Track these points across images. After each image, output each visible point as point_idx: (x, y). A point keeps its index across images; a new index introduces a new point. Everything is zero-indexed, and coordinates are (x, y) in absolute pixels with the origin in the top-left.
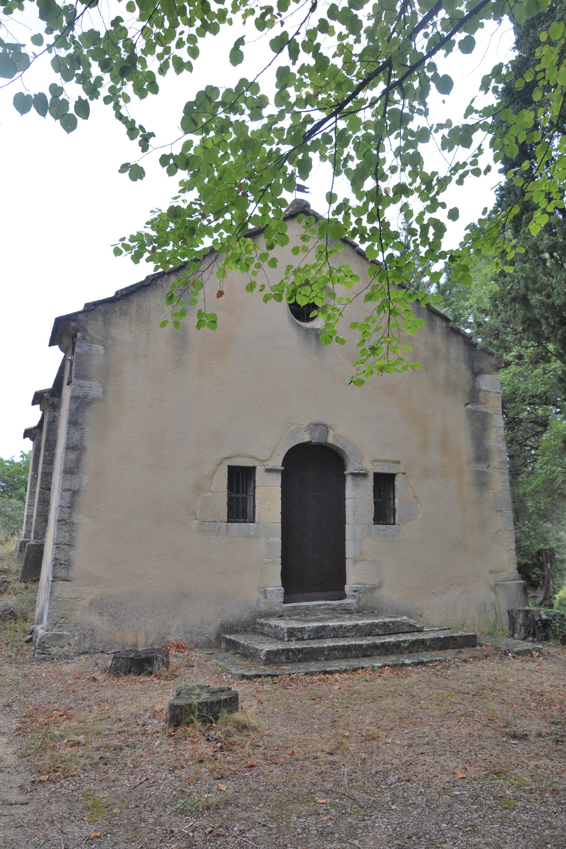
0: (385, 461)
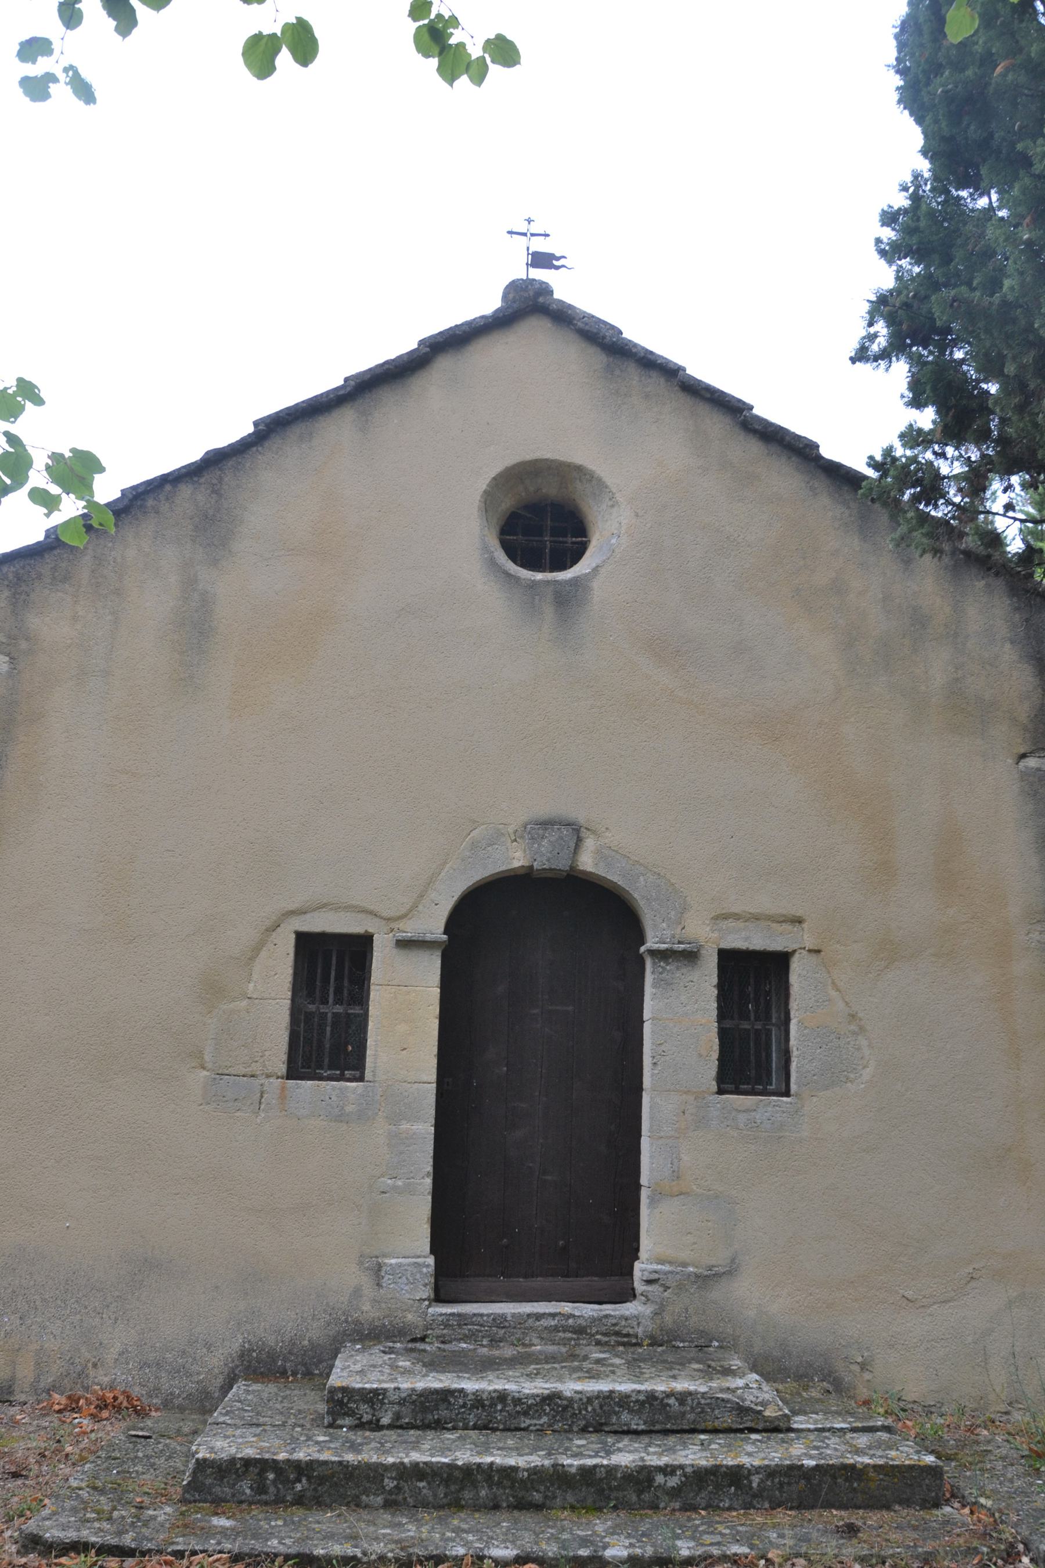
0: (756, 918)
